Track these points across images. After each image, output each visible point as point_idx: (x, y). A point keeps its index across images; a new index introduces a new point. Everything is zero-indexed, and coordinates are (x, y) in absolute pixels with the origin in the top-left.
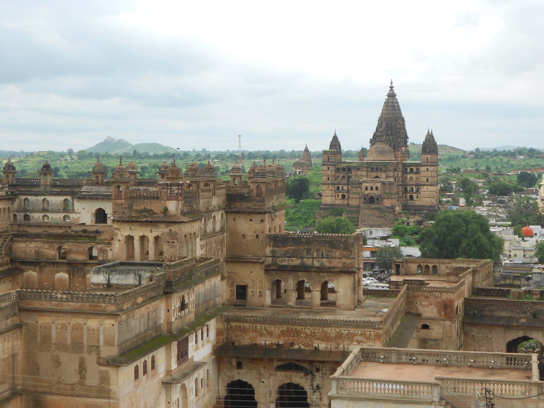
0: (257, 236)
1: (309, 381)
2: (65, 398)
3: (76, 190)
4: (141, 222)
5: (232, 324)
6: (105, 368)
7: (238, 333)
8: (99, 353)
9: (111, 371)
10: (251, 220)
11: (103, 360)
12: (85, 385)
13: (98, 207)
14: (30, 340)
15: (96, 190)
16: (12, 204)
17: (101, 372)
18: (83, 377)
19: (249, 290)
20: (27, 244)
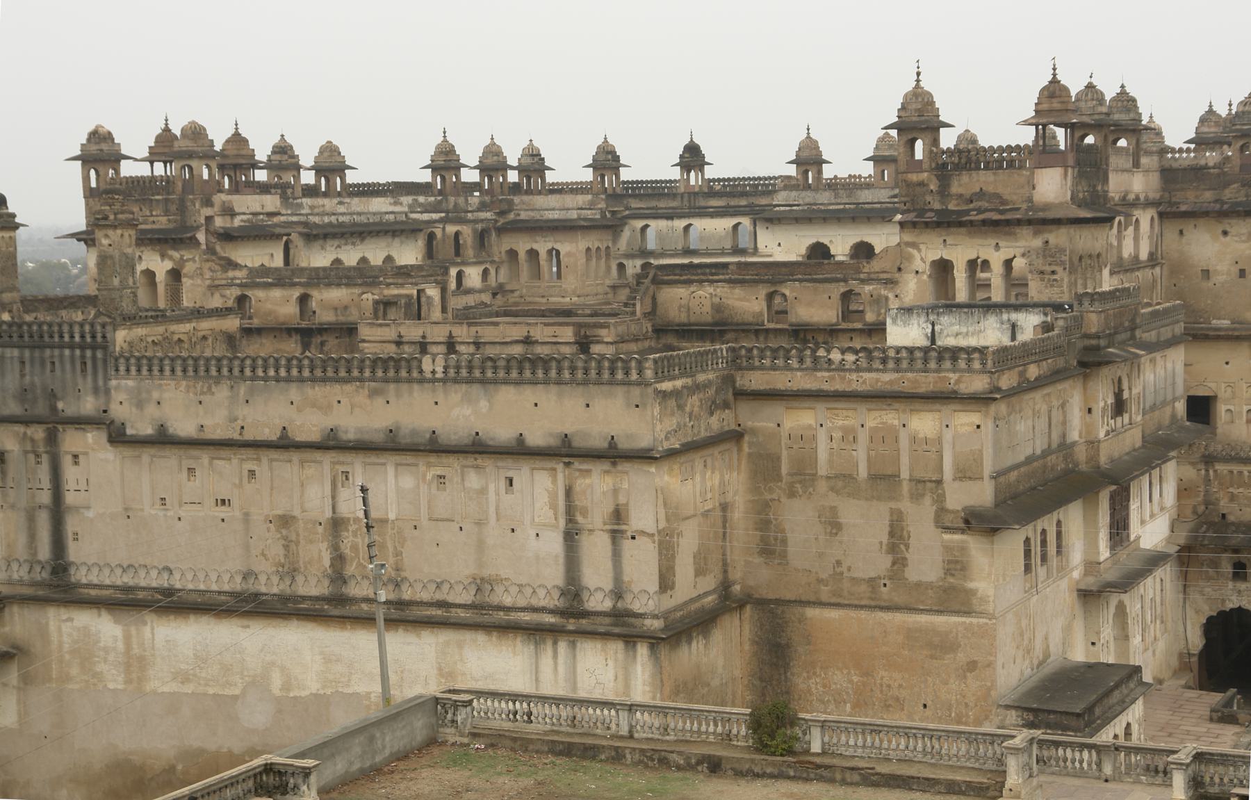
2: (853, 613)
3: (764, 201)
4: (971, 222)
5: (1221, 468)
6: (957, 537)
7: (1235, 491)
8: (940, 499)
9: (974, 545)
10: (1225, 233)
11: (951, 517)
13: (814, 241)
14: (765, 469)
15: (807, 200)
16: (615, 241)
17: (947, 548)
18: (899, 563)
19: (1221, 409)
20: (692, 289)
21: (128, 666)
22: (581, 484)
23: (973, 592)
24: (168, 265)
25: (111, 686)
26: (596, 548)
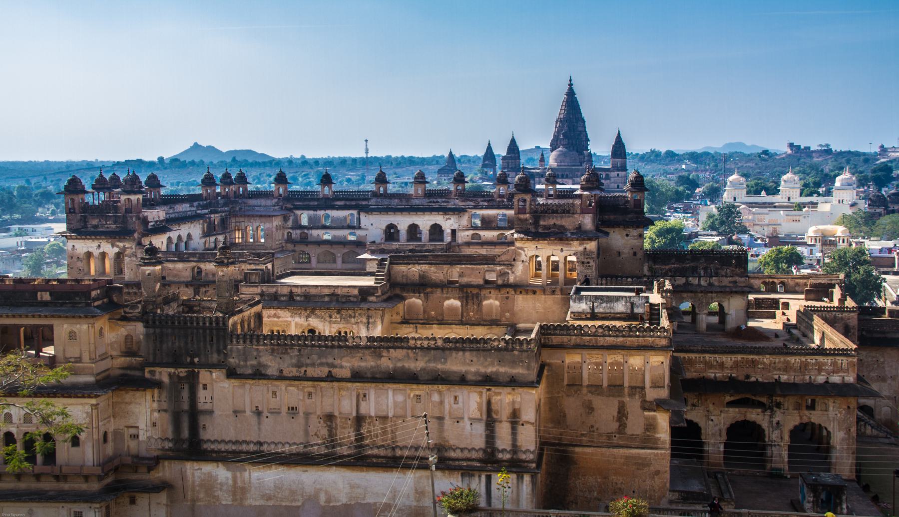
0: (635, 254)
1: (767, 417)
6: (652, 413)
10: (627, 235)
12: (625, 434)
17: (646, 418)
18: (622, 426)
21: (234, 494)
22: (495, 399)
23: (659, 439)
24: (116, 250)
25: (224, 503)
26: (503, 430)
